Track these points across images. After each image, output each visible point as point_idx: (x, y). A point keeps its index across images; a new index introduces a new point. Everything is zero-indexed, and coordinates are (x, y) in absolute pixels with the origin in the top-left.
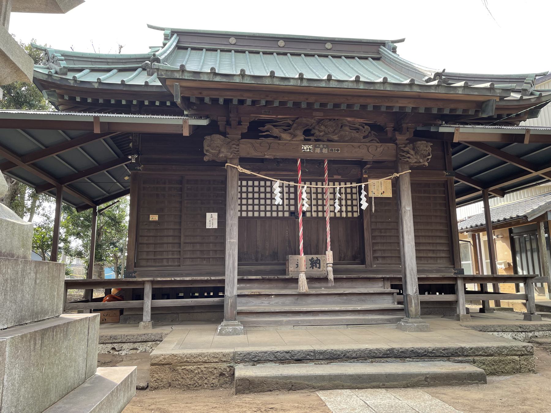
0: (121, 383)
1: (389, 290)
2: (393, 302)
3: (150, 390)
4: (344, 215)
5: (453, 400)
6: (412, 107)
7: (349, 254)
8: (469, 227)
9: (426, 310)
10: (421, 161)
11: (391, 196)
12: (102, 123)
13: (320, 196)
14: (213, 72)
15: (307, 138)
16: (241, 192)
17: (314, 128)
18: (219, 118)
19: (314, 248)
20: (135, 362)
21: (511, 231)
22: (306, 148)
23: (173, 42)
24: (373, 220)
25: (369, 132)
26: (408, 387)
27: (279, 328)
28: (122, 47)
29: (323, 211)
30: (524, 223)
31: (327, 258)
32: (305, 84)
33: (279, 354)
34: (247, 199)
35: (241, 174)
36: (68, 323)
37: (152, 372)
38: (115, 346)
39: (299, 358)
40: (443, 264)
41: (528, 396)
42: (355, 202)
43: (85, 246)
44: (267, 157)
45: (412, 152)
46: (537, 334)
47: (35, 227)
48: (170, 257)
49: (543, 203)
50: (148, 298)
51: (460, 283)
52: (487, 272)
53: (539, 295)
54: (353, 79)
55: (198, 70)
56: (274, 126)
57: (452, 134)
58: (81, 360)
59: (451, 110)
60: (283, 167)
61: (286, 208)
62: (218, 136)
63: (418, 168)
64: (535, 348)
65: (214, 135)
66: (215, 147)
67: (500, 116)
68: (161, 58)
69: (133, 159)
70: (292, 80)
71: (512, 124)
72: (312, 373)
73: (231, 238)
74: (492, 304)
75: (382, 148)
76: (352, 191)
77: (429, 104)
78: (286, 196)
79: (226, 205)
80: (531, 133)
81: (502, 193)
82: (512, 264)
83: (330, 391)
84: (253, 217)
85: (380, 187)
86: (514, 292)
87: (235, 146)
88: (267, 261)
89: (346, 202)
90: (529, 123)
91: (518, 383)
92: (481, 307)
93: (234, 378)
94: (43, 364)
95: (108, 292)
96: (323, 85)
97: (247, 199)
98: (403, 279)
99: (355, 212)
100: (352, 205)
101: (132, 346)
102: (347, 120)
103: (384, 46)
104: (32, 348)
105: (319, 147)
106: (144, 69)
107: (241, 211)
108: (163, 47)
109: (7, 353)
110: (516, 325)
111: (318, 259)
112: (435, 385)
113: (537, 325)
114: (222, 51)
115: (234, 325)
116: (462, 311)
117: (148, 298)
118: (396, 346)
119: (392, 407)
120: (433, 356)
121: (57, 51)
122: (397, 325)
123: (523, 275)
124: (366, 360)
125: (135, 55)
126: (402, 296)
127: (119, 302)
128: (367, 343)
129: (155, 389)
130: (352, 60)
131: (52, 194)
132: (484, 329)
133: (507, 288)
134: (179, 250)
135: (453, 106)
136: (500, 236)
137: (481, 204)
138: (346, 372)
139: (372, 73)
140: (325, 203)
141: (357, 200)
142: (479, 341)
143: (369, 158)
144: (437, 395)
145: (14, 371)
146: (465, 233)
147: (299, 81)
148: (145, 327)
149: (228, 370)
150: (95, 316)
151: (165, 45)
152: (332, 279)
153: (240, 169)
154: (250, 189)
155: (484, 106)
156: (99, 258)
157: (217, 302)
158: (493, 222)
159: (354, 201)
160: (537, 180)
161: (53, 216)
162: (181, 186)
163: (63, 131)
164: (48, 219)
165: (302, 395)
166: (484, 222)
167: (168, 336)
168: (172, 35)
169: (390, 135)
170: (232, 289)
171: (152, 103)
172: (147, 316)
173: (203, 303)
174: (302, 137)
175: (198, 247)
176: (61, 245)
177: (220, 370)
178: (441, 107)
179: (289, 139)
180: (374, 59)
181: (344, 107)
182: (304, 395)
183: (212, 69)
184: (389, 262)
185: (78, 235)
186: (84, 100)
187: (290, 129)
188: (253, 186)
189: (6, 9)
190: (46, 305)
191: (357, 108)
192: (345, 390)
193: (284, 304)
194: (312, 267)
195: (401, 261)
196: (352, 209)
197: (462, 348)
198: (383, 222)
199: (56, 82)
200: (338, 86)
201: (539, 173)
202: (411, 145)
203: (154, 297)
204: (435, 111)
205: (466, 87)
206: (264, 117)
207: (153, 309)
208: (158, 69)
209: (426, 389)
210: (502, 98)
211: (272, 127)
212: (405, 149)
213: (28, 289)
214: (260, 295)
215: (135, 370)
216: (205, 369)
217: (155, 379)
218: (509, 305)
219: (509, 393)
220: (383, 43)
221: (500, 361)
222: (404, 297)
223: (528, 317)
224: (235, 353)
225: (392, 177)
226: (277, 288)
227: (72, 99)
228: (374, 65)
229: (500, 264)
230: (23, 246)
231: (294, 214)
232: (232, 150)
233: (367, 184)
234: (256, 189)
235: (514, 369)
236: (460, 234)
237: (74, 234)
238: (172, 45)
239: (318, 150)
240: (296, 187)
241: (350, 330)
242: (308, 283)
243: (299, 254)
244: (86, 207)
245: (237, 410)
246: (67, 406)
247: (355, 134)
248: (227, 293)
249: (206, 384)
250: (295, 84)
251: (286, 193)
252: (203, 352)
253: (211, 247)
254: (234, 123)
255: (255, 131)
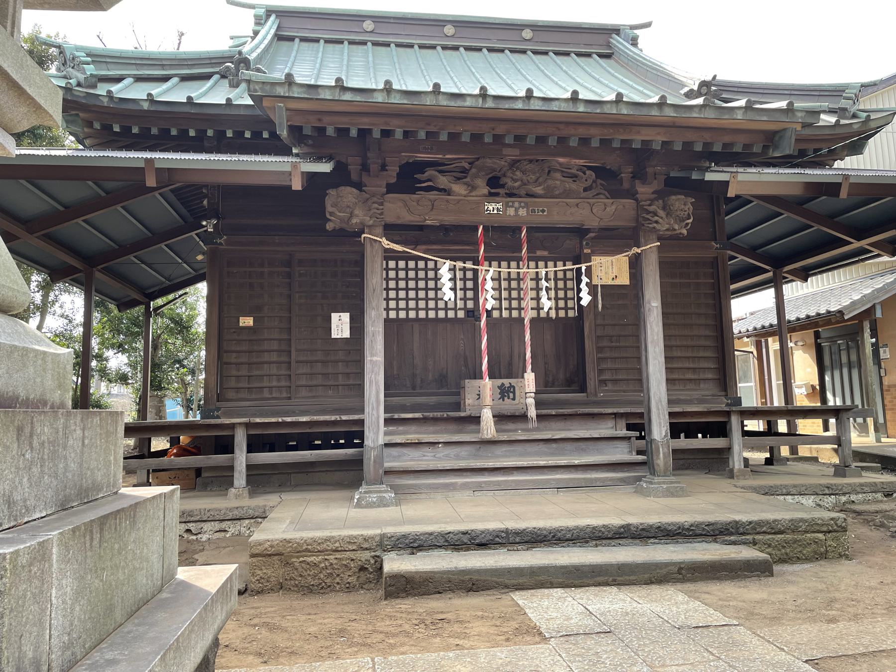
0: (218, 591)
1: (624, 432)
2: (630, 452)
3: (250, 595)
4: (505, 314)
5: (721, 603)
6: (663, 142)
7: (561, 376)
8: (751, 329)
9: (681, 462)
10: (676, 227)
11: (628, 283)
12: (159, 171)
13: (514, 284)
14: (340, 86)
15: (493, 191)
16: (387, 279)
17: (504, 175)
18: (350, 160)
19: (505, 368)
20: (224, 551)
21: (817, 335)
22: (492, 207)
23: (269, 29)
24: (598, 322)
25: (594, 181)
26: (652, 583)
27: (450, 494)
28: (183, 34)
29: (520, 309)
30: (838, 322)
31: (526, 383)
32: (490, 104)
33: (451, 535)
34: (397, 289)
35: (387, 250)
36: (137, 504)
37: (253, 567)
38: (191, 526)
39: (484, 541)
40: (709, 389)
41: (837, 595)
42: (570, 294)
43: (133, 366)
44: (429, 222)
45: (661, 213)
46: (853, 497)
47: (49, 335)
48: (275, 384)
49: (868, 291)
50: (241, 451)
51: (735, 421)
52: (778, 401)
53: (859, 436)
54: (568, 95)
55: (312, 82)
56: (440, 172)
57: (726, 184)
58: (155, 558)
59: (725, 145)
60: (454, 240)
61: (460, 304)
62: (348, 189)
63: (671, 238)
64: (850, 520)
65: (343, 188)
66: (344, 207)
67: (802, 153)
68: (252, 57)
69: (209, 225)
70: (468, 99)
71: (820, 165)
72: (503, 564)
73: (372, 355)
74: (785, 451)
75: (614, 207)
76: (565, 275)
77: (690, 136)
78: (459, 284)
79: (363, 300)
80: (852, 180)
81: (804, 275)
82: (818, 387)
83: (532, 591)
84: (407, 319)
85: (611, 269)
86: (820, 432)
87: (376, 205)
88: (430, 384)
89: (556, 293)
90: (849, 164)
91: (823, 574)
92: (768, 455)
93: (382, 573)
94: (104, 569)
95: (174, 442)
96: (519, 105)
97: (397, 289)
98: (645, 415)
99: (571, 309)
100: (566, 299)
101: (217, 526)
102: (557, 162)
103: (618, 34)
104: (88, 545)
105: (512, 207)
106: (223, 77)
107: (387, 309)
108: (253, 38)
109: (54, 556)
110: (820, 485)
111: (511, 386)
112: (693, 580)
113: (855, 484)
114: (351, 43)
115: (380, 492)
116: (737, 464)
117: (241, 451)
118: (633, 520)
119: (627, 614)
120: (690, 536)
121: (78, 49)
122: (636, 488)
123: (835, 406)
124: (587, 542)
125: (208, 52)
126: (644, 442)
127: (194, 456)
128: (589, 517)
129: (258, 593)
130: (566, 58)
131: (77, 282)
132: (770, 492)
133: (809, 426)
134: (288, 373)
135: (727, 139)
136: (800, 343)
137: (770, 293)
138: (557, 562)
139: (598, 80)
140: (522, 296)
141: (573, 299)
142: (763, 511)
143: (593, 223)
144: (697, 595)
145: (64, 582)
146: (745, 339)
147: (480, 100)
148: (237, 496)
149: (372, 562)
150: (173, 491)
151: (256, 33)
152: (534, 417)
153: (386, 243)
154: (402, 274)
155: (777, 138)
156: (158, 386)
157: (352, 455)
158: (789, 322)
159: (569, 301)
160: (859, 255)
161: (79, 318)
162: (288, 269)
163: (95, 183)
164: (70, 322)
165: (488, 598)
166: (775, 322)
167: (276, 510)
168: (268, 16)
169: (626, 185)
170: (376, 434)
171: (239, 134)
172: (240, 478)
173: (329, 457)
174: (485, 190)
175: (319, 368)
176: (94, 363)
177: (360, 563)
178: (709, 141)
179: (464, 192)
180: (601, 56)
181: (552, 141)
182: (491, 598)
183: (338, 80)
184: (624, 388)
185: (120, 348)
186: (126, 130)
187: (465, 177)
188: (407, 269)
189: (15, 8)
190: (99, 475)
191: (573, 143)
192: (555, 590)
193: (458, 457)
194: (503, 398)
195: (642, 386)
196: (566, 303)
197: (736, 522)
198: (615, 325)
199: (79, 100)
200: (543, 108)
201: (864, 243)
202: (661, 201)
203: (251, 448)
204: (698, 148)
205: (749, 107)
206: (422, 156)
207: (249, 467)
208: (249, 82)
209: (679, 586)
210: (805, 125)
211: (437, 173)
212: (652, 208)
213: (73, 455)
214: (419, 444)
215: (236, 569)
216: (335, 561)
217: (258, 578)
218: (811, 452)
219: (808, 591)
220: (616, 30)
221: (795, 541)
222: (647, 445)
223: (840, 470)
224: (383, 536)
225: (630, 253)
226: (447, 432)
227: (107, 128)
228: (602, 67)
229: (800, 387)
230: (60, 386)
231: (473, 314)
232: (372, 211)
233: (590, 266)
234: (412, 274)
235: (815, 553)
236: (736, 341)
237: (113, 346)
238: (268, 33)
239: (511, 212)
240: (476, 272)
241: (563, 496)
242: (496, 423)
243: (481, 378)
244: (133, 304)
245: (388, 623)
246: (141, 629)
247: (570, 185)
248: (368, 442)
249: (338, 583)
250: (474, 105)
251: (460, 279)
252: (333, 534)
253: (341, 368)
254: (374, 168)
255: (409, 180)
